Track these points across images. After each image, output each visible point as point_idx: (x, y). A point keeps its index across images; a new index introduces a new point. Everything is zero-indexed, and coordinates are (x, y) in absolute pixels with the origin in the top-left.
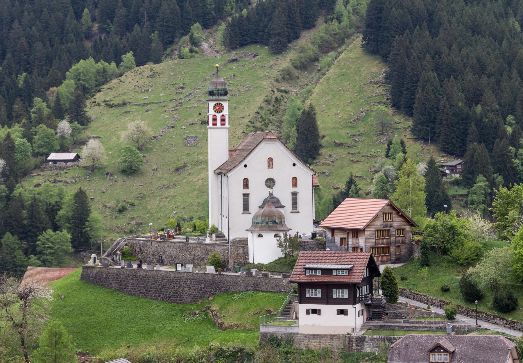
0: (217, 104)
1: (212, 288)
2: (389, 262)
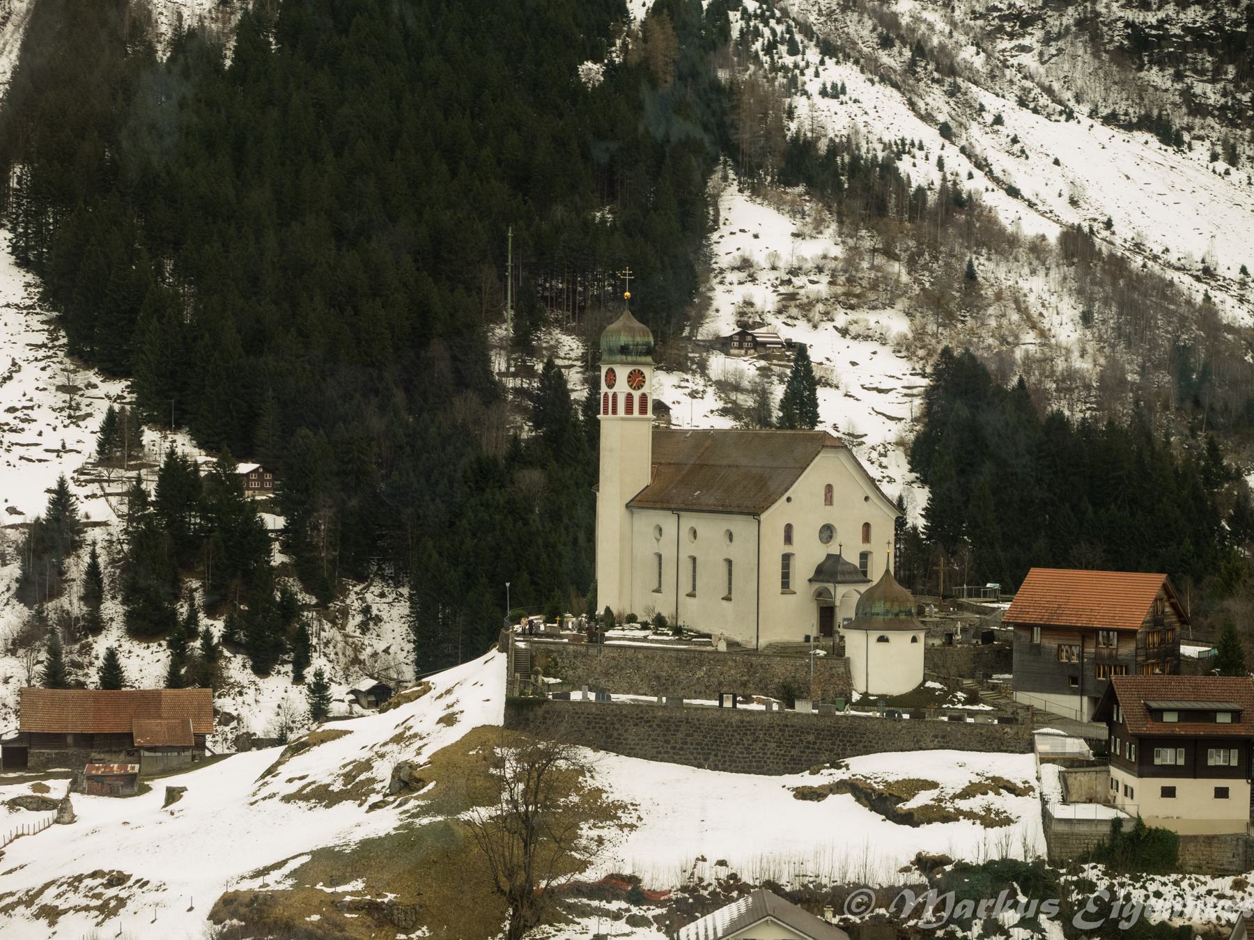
1: (833, 744)
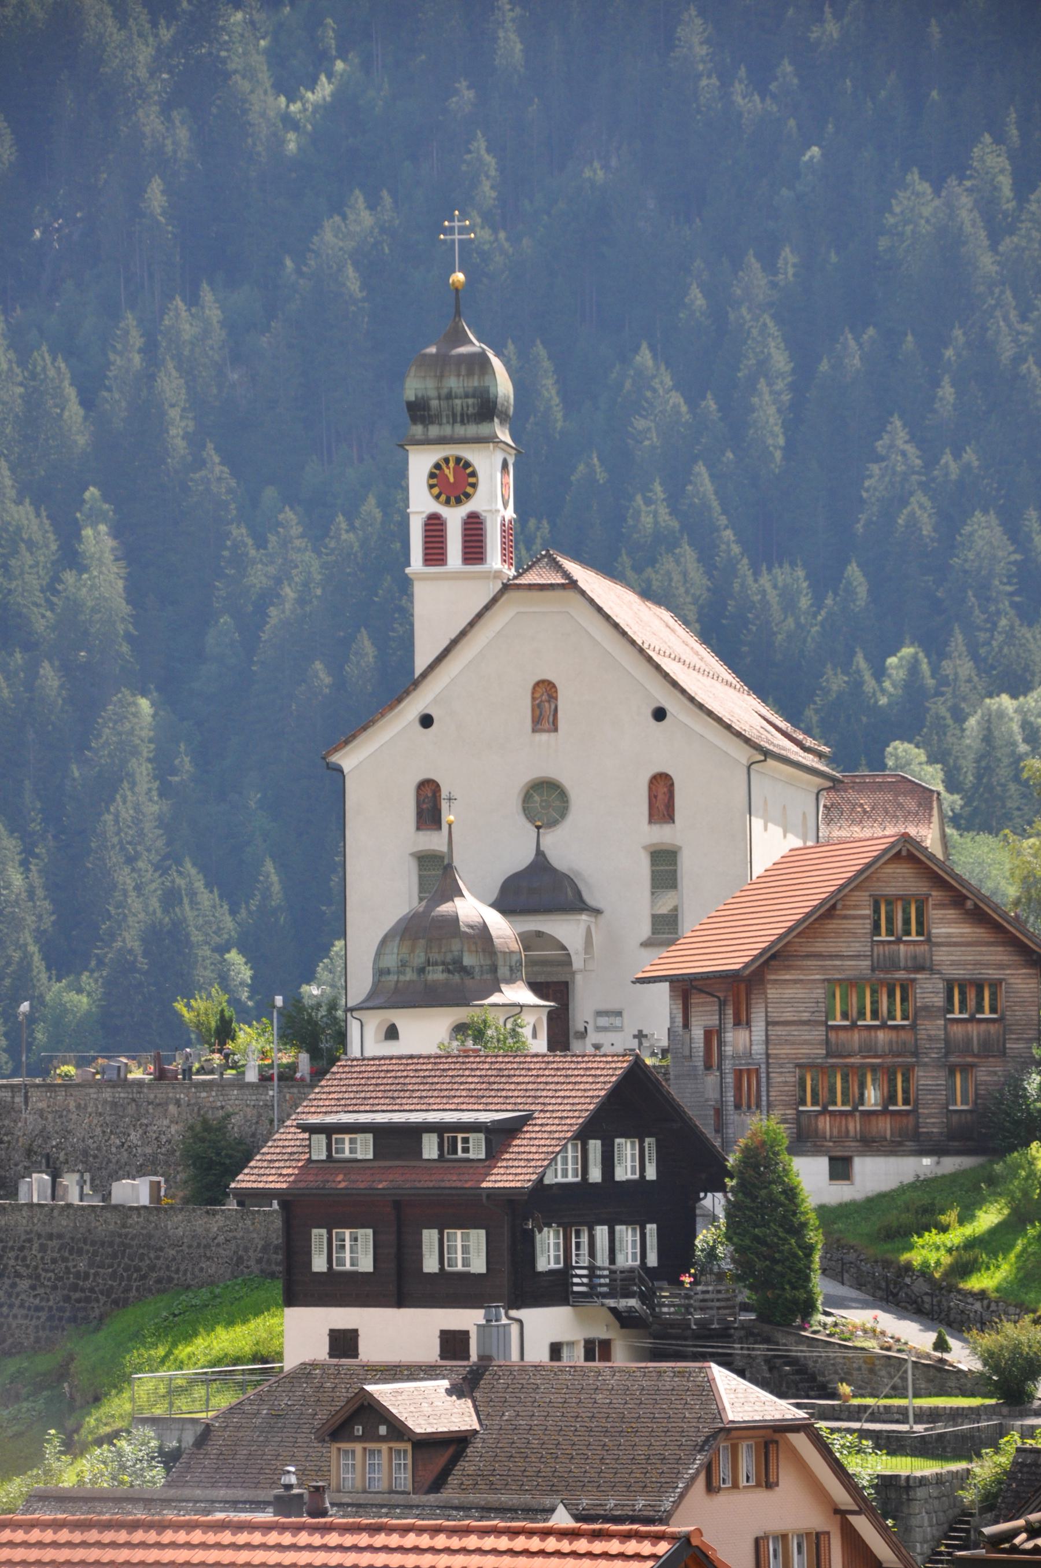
0: (447, 460)
2: (910, 1145)
